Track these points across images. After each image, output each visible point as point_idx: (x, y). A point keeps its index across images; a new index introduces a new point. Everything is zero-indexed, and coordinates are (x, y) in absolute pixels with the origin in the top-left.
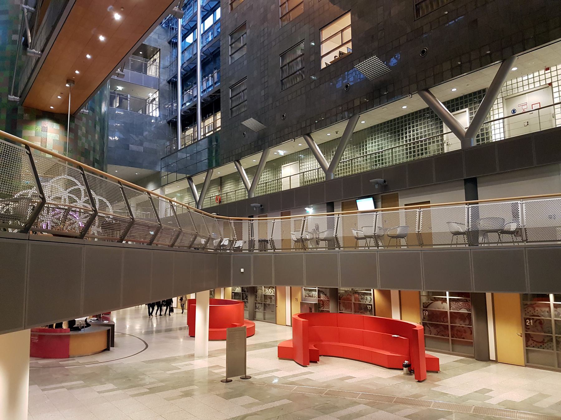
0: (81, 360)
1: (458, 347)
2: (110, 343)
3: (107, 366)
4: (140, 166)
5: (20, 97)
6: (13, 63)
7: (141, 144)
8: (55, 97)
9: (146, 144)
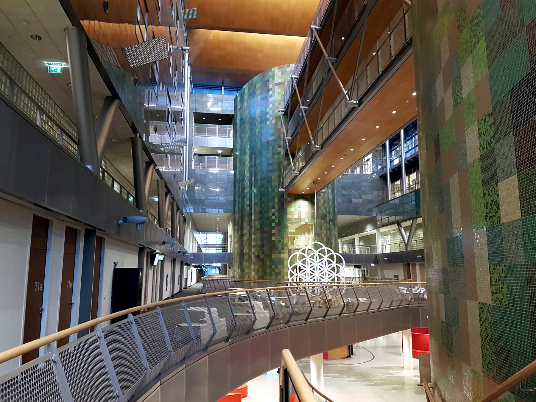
0: (335, 362)
2: (350, 353)
3: (350, 367)
4: (360, 214)
5: (285, 188)
6: (279, 166)
7: (360, 197)
8: (304, 184)
9: (364, 197)
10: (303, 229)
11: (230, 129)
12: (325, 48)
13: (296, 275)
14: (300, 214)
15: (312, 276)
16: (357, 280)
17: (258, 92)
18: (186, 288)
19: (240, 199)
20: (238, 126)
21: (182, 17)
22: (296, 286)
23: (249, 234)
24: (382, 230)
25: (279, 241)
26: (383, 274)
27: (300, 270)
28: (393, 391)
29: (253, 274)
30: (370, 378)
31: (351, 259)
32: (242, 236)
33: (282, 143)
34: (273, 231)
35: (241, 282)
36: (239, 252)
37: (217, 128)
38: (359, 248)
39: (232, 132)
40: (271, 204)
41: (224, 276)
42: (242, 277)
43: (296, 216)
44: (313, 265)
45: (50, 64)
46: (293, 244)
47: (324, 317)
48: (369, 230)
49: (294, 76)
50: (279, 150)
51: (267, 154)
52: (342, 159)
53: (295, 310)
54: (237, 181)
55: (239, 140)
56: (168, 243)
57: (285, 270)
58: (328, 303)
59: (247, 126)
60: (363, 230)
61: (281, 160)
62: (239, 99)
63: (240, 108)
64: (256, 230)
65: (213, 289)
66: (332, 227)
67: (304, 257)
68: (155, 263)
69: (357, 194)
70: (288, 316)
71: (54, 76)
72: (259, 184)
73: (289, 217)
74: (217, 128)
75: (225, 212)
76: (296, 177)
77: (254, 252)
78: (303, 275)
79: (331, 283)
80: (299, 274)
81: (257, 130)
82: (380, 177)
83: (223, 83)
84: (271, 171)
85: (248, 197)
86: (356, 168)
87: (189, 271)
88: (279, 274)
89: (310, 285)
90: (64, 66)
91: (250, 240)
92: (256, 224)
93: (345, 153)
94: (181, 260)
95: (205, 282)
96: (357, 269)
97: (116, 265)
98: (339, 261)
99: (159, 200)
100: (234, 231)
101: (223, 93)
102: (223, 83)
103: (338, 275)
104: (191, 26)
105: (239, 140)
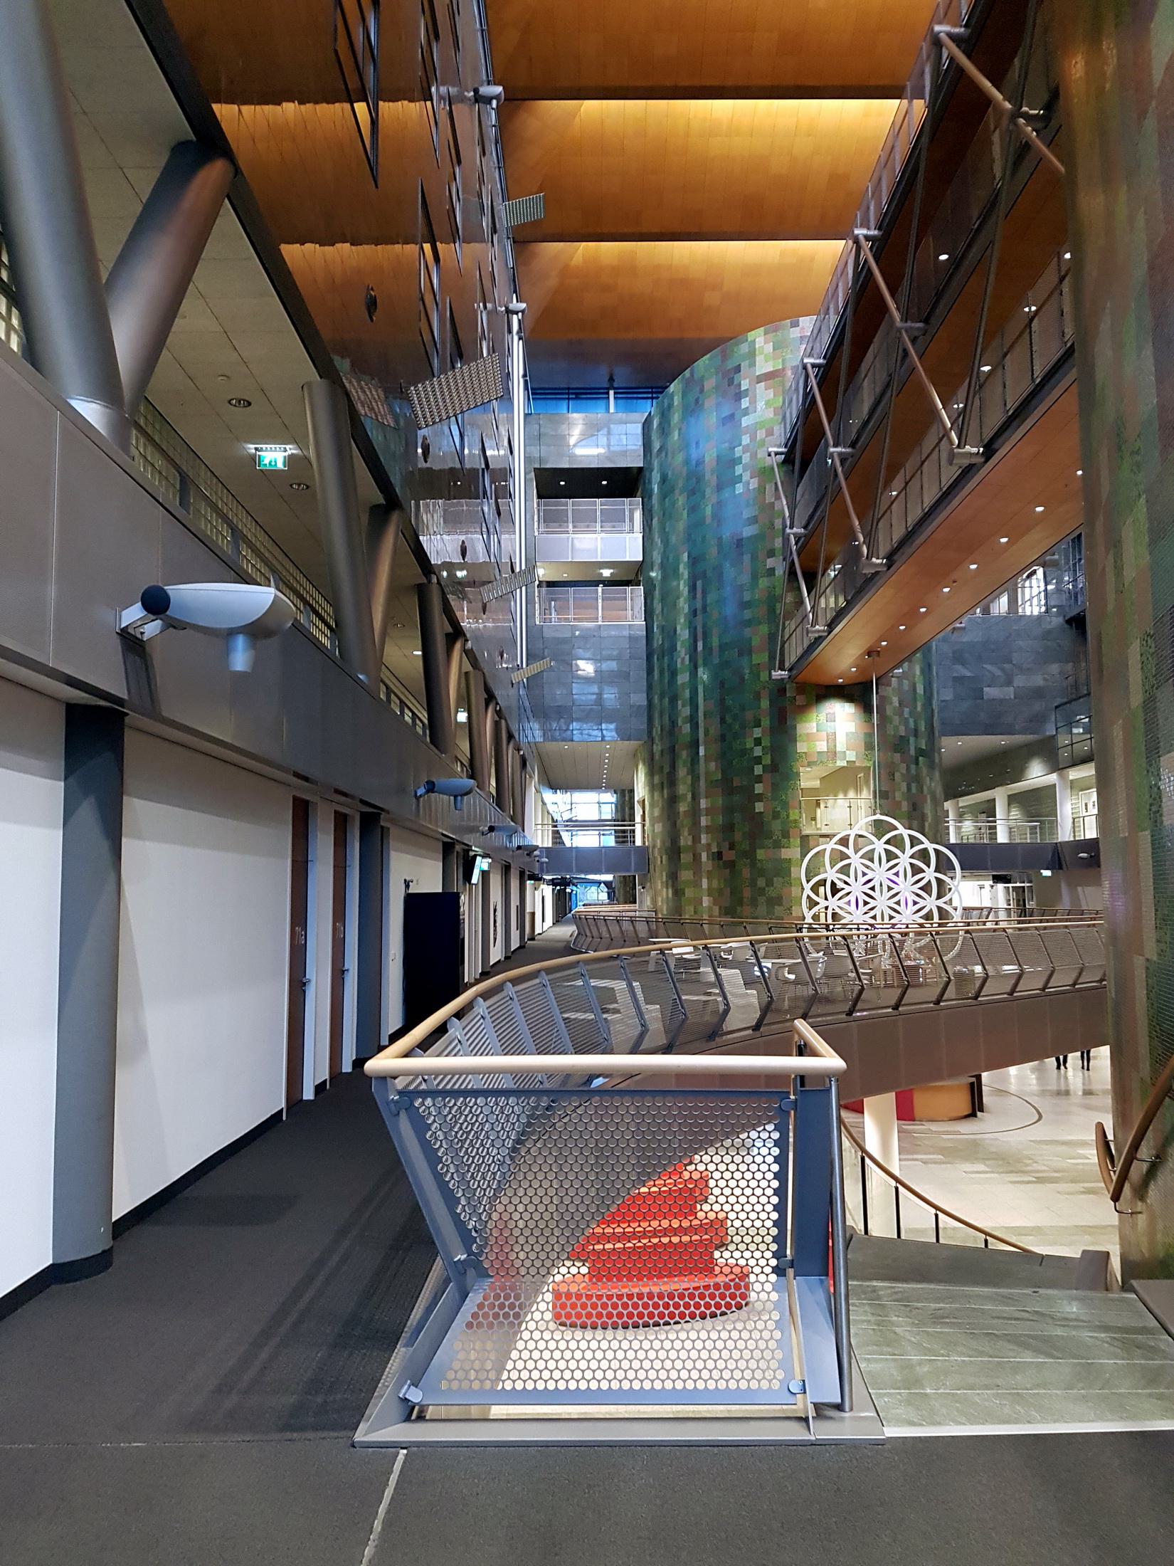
0: (934, 1127)
1: (563, 945)
2: (976, 1106)
4: (1010, 732)
5: (790, 670)
6: (772, 610)
7: (1009, 683)
9: (1019, 681)
10: (842, 779)
11: (633, 509)
12: (893, 296)
13: (823, 903)
14: (832, 738)
15: (869, 907)
16: (1002, 915)
17: (709, 403)
18: (533, 939)
19: (667, 700)
20: (655, 500)
21: (503, 222)
22: (825, 933)
23: (694, 798)
24: (1074, 774)
25: (776, 815)
26: (1075, 899)
27: (835, 890)
28: (1083, 1196)
29: (706, 901)
30: (1027, 1165)
31: (976, 859)
32: (672, 801)
33: (778, 543)
34: (759, 788)
35: (676, 925)
36: (668, 844)
37: (599, 507)
38: (1007, 827)
39: (638, 515)
40: (749, 715)
41: (627, 907)
42: (677, 909)
43: (822, 746)
44: (867, 875)
45: (261, 450)
46: (814, 819)
47: (896, 1007)
48: (1037, 775)
49: (812, 361)
50: (770, 563)
51: (736, 575)
52: (946, 590)
53: (823, 990)
54: (655, 651)
55: (658, 540)
56: (501, 829)
57: (795, 891)
58: (907, 977)
59: (681, 500)
60: (1018, 776)
61: (778, 591)
62: (655, 423)
63: (660, 450)
64: (712, 784)
65: (606, 941)
66: (925, 771)
67: (844, 856)
68: (474, 880)
69: (999, 673)
70: (803, 1005)
71: (270, 475)
72: (716, 661)
73: (801, 747)
74: (599, 507)
75: (624, 735)
76: (819, 640)
77: (709, 845)
78: (841, 903)
79: (921, 925)
80: (833, 903)
81: (709, 511)
82: (1069, 622)
83: (611, 379)
84: (748, 623)
85: (687, 694)
86: (998, 597)
87: (538, 894)
88: (778, 900)
89: (862, 931)
90: (289, 452)
91: (695, 813)
92: (709, 768)
93: (954, 576)
94: (522, 867)
95: (577, 920)
96: (1000, 886)
97: (407, 886)
98: (944, 865)
99: (469, 718)
100: (652, 787)
101: (612, 410)
102: (611, 379)
103: (940, 903)
104: (524, 239)
105: (658, 540)
